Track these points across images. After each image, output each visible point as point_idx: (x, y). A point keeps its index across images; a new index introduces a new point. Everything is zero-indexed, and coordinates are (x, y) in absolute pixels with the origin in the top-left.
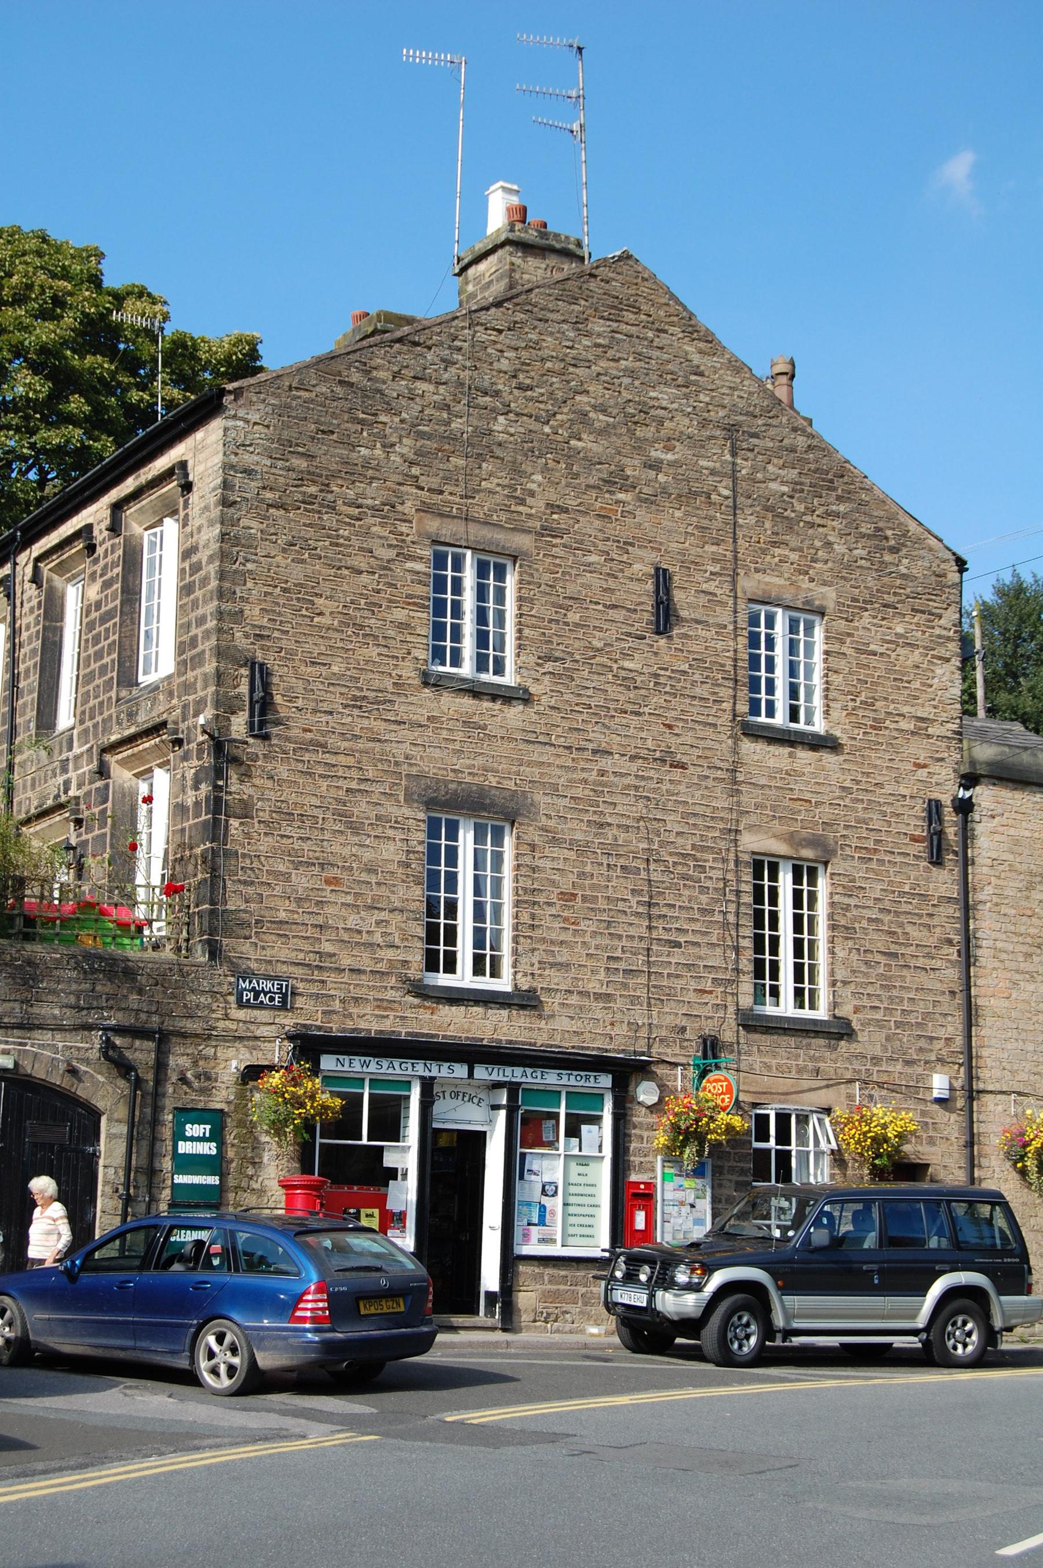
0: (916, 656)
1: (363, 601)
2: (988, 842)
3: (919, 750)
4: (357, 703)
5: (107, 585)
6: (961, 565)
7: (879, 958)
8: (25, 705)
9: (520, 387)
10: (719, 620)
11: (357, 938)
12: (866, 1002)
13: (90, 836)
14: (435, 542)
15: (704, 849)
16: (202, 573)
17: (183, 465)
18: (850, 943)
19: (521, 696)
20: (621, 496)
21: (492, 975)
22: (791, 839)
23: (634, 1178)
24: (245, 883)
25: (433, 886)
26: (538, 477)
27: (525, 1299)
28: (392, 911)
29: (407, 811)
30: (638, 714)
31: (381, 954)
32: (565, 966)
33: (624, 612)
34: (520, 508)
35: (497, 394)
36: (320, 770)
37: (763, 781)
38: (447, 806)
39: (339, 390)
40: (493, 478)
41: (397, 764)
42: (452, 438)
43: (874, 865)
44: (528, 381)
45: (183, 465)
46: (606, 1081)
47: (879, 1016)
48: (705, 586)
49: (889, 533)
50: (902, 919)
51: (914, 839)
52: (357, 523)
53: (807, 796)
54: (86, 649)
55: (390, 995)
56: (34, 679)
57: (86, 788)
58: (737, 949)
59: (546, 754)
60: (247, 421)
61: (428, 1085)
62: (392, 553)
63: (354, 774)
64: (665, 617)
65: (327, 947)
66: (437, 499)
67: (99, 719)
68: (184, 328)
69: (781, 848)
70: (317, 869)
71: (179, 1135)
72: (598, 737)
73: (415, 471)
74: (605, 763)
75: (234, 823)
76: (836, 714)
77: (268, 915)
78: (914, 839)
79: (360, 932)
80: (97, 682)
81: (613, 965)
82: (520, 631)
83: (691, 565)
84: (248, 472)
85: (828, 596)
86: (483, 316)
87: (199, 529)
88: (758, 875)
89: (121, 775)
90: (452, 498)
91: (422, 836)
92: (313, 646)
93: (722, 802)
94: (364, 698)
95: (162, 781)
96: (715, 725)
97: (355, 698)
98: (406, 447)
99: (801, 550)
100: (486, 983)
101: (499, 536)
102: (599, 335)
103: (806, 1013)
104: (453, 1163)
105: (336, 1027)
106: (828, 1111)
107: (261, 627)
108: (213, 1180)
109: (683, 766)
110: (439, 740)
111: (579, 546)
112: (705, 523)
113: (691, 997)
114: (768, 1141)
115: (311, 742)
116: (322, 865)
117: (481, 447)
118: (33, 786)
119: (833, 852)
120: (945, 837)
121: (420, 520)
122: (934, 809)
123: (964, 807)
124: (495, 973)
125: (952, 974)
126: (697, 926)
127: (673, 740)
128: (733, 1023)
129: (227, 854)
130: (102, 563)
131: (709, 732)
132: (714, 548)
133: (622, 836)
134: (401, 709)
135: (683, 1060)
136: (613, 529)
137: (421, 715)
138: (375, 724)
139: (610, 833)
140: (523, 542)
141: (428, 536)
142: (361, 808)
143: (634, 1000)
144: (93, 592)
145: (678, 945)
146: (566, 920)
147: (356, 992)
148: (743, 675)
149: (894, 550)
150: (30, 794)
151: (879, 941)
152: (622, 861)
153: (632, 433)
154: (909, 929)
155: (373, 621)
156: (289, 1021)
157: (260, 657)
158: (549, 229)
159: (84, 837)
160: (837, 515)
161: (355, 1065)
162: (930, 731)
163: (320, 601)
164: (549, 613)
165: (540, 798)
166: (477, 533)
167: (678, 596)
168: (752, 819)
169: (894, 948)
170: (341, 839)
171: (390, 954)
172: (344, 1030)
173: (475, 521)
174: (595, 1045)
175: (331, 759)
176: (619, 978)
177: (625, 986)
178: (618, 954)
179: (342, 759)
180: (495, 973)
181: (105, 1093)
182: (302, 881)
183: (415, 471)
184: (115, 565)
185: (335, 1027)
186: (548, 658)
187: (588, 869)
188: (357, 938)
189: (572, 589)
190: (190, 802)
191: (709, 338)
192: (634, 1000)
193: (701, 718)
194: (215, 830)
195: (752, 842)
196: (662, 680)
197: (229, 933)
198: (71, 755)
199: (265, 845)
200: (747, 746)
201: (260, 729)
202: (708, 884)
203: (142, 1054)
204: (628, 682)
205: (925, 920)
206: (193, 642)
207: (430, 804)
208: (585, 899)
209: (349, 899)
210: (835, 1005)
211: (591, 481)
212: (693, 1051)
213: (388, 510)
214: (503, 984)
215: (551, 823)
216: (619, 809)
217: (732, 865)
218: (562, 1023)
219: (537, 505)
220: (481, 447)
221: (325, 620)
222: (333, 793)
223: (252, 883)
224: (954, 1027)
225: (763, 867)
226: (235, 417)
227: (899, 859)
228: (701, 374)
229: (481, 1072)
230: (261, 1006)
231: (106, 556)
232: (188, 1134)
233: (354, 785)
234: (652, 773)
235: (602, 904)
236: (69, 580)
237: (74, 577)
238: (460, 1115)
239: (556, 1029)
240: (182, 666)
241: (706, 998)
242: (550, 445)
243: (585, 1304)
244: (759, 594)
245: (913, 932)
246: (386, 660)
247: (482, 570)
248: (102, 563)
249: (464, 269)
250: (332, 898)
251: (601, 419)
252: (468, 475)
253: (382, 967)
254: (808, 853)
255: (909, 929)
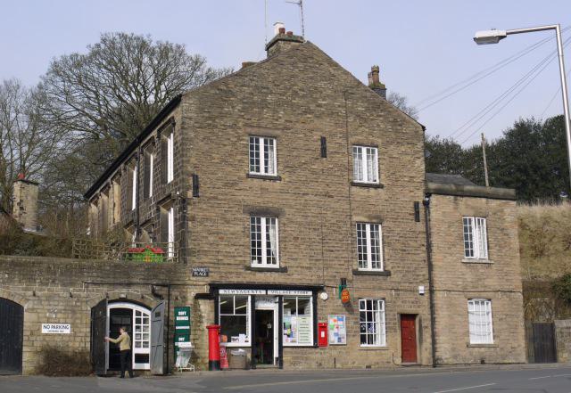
0: (409, 158)
4: (226, 185)
6: (424, 128)
17: (173, 117)
20: (310, 116)
22: (369, 217)
23: (320, 322)
25: (253, 238)
35: (268, 88)
38: (256, 213)
40: (267, 114)
45: (173, 117)
46: (310, 293)
47: (400, 269)
59: (288, 196)
61: (253, 297)
62: (235, 139)
63: (227, 206)
64: (324, 153)
65: (220, 258)
66: (250, 122)
69: (366, 220)
71: (176, 315)
72: (304, 190)
73: (243, 114)
74: (307, 197)
75: (190, 223)
76: (383, 176)
83: (333, 135)
84: (190, 119)
85: (379, 141)
86: (263, 65)
88: (359, 228)
89: (163, 210)
90: (254, 120)
92: (212, 169)
100: (271, 266)
103: (376, 270)
104: (262, 318)
105: (224, 281)
108: (188, 327)
119: (383, 220)
120: (420, 212)
122: (416, 205)
123: (426, 204)
124: (274, 263)
125: (424, 255)
133: (313, 219)
140: (278, 132)
141: (247, 133)
142: (229, 216)
143: (319, 268)
145: (332, 251)
151: (398, 246)
153: (312, 96)
156: (208, 280)
157: (196, 173)
160: (381, 116)
161: (230, 292)
163: (214, 155)
164: (287, 154)
166: (262, 131)
167: (328, 144)
171: (240, 259)
174: (305, 282)
175: (219, 202)
179: (223, 202)
180: (274, 263)
182: (211, 239)
183: (243, 114)
186: (288, 167)
189: (294, 146)
192: (319, 268)
199: (199, 228)
201: (196, 194)
204: (313, 173)
207: (251, 213)
210: (384, 267)
212: (339, 284)
215: (291, 216)
217: (349, 226)
218: (295, 276)
219: (282, 121)
220: (264, 105)
221: (217, 161)
224: (425, 272)
229: (270, 292)
239: (295, 278)
245: (411, 243)
251: (301, 93)
252: (260, 113)
253: (237, 262)
254: (374, 221)
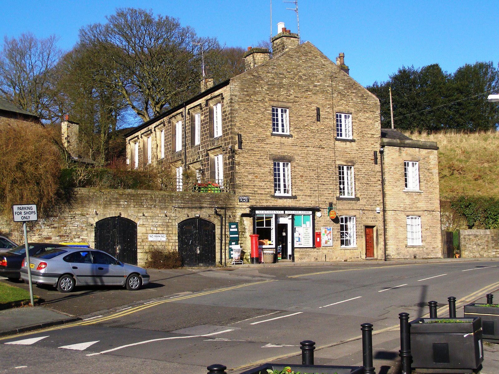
0: (371, 121)
1: (259, 120)
2: (387, 160)
3: (371, 141)
4: (258, 141)
5: (205, 117)
7: (365, 184)
8: (188, 139)
9: (288, 72)
10: (330, 117)
11: (261, 187)
12: (362, 193)
13: (205, 168)
14: (272, 107)
15: (329, 165)
16: (228, 116)
18: (359, 182)
19: (291, 136)
21: (288, 193)
22: (346, 161)
24: (240, 178)
26: (292, 91)
27: (296, 255)
28: (268, 181)
29: (269, 162)
30: (314, 138)
31: (266, 190)
33: (311, 117)
34: (289, 98)
35: (283, 74)
36: (252, 155)
37: (340, 150)
38: (277, 160)
39: (252, 77)
41: (267, 152)
43: (363, 166)
44: (290, 71)
45: (222, 94)
46: (311, 212)
48: (327, 111)
49: (365, 95)
50: (370, 176)
51: (372, 160)
52: (257, 104)
53: (349, 152)
54: (202, 129)
55: (269, 198)
56: (190, 134)
57: (204, 158)
59: (297, 148)
60: (234, 86)
62: (264, 110)
65: (256, 190)
66: (272, 97)
67: (206, 144)
69: (345, 164)
70: (253, 174)
71: (230, 228)
73: (268, 92)
74: (308, 149)
76: (355, 134)
77: (244, 184)
78: (372, 160)
79: (262, 186)
80: (205, 136)
81: (311, 189)
82: (290, 123)
85: (353, 110)
87: (226, 107)
88: (340, 169)
90: (275, 96)
91: (273, 166)
92: (250, 130)
94: (260, 139)
95: (221, 157)
96: (330, 139)
97: (258, 140)
99: (346, 101)
100: (286, 195)
101: (285, 104)
102: (303, 59)
105: (258, 205)
106: (355, 216)
107: (239, 127)
108: (237, 236)
109: (324, 148)
110: (275, 146)
111: (301, 104)
112: (327, 97)
113: (327, 195)
114: (343, 223)
115: (251, 149)
116: (254, 174)
117: (281, 86)
118: (191, 157)
119: (355, 164)
121: (269, 102)
122: (375, 153)
123: (382, 152)
125: (380, 187)
126: (328, 181)
127: (321, 143)
128: (336, 200)
129: (236, 173)
130: (204, 112)
131: (329, 141)
132: (329, 102)
134: (267, 141)
135: (326, 208)
136: (308, 100)
137: (271, 142)
138: (261, 143)
139: (309, 163)
140: (290, 105)
142: (260, 162)
144: (203, 117)
145: (324, 185)
146: (302, 181)
147: (262, 198)
148: (335, 128)
149: (366, 99)
150: (190, 158)
151: (364, 181)
152: (312, 168)
153: (311, 79)
154: (371, 178)
155: (261, 124)
156: (249, 204)
157: (240, 133)
158: (291, 32)
159: (204, 168)
160: (354, 93)
162: (374, 137)
165: (296, 157)
166: (280, 104)
167: (321, 113)
168: (338, 158)
169: (368, 182)
170: (257, 168)
171: (268, 190)
172: (260, 206)
173: (280, 101)
174: (308, 205)
175: (254, 152)
176: (312, 192)
177: (314, 193)
178: (312, 187)
179: (257, 152)
181: (216, 221)
182: (250, 177)
184: (207, 112)
185: (258, 205)
186: (296, 128)
187: (306, 170)
188: (261, 187)
189: (300, 113)
190: (228, 162)
191: (326, 58)
193: (327, 138)
194: (232, 168)
195: (338, 163)
196: (319, 131)
197: (237, 188)
198: (200, 151)
199: (243, 170)
200: (337, 142)
201: (240, 147)
202: (330, 172)
203: (222, 212)
205: (374, 176)
206: (226, 130)
207: (274, 160)
208: (305, 176)
209: (259, 180)
210: (355, 195)
211: (303, 91)
213: (263, 101)
214: (290, 195)
215: (298, 162)
216: (312, 158)
218: (302, 202)
219: (292, 97)
220: (281, 86)
222: (255, 159)
223: (241, 178)
224: (380, 198)
225: (340, 168)
226: (232, 85)
227: (368, 164)
228: (325, 65)
231: (205, 110)
232: (232, 227)
233: (259, 157)
234: (317, 150)
235: (309, 177)
236: (196, 114)
237: (197, 113)
238: (282, 221)
241: (330, 195)
242: (294, 84)
243: (308, 256)
244: (338, 111)
246: (264, 131)
247: (282, 111)
248: (204, 112)
249: (273, 41)
250: (256, 180)
251: (304, 77)
253: (266, 193)
255: (371, 178)
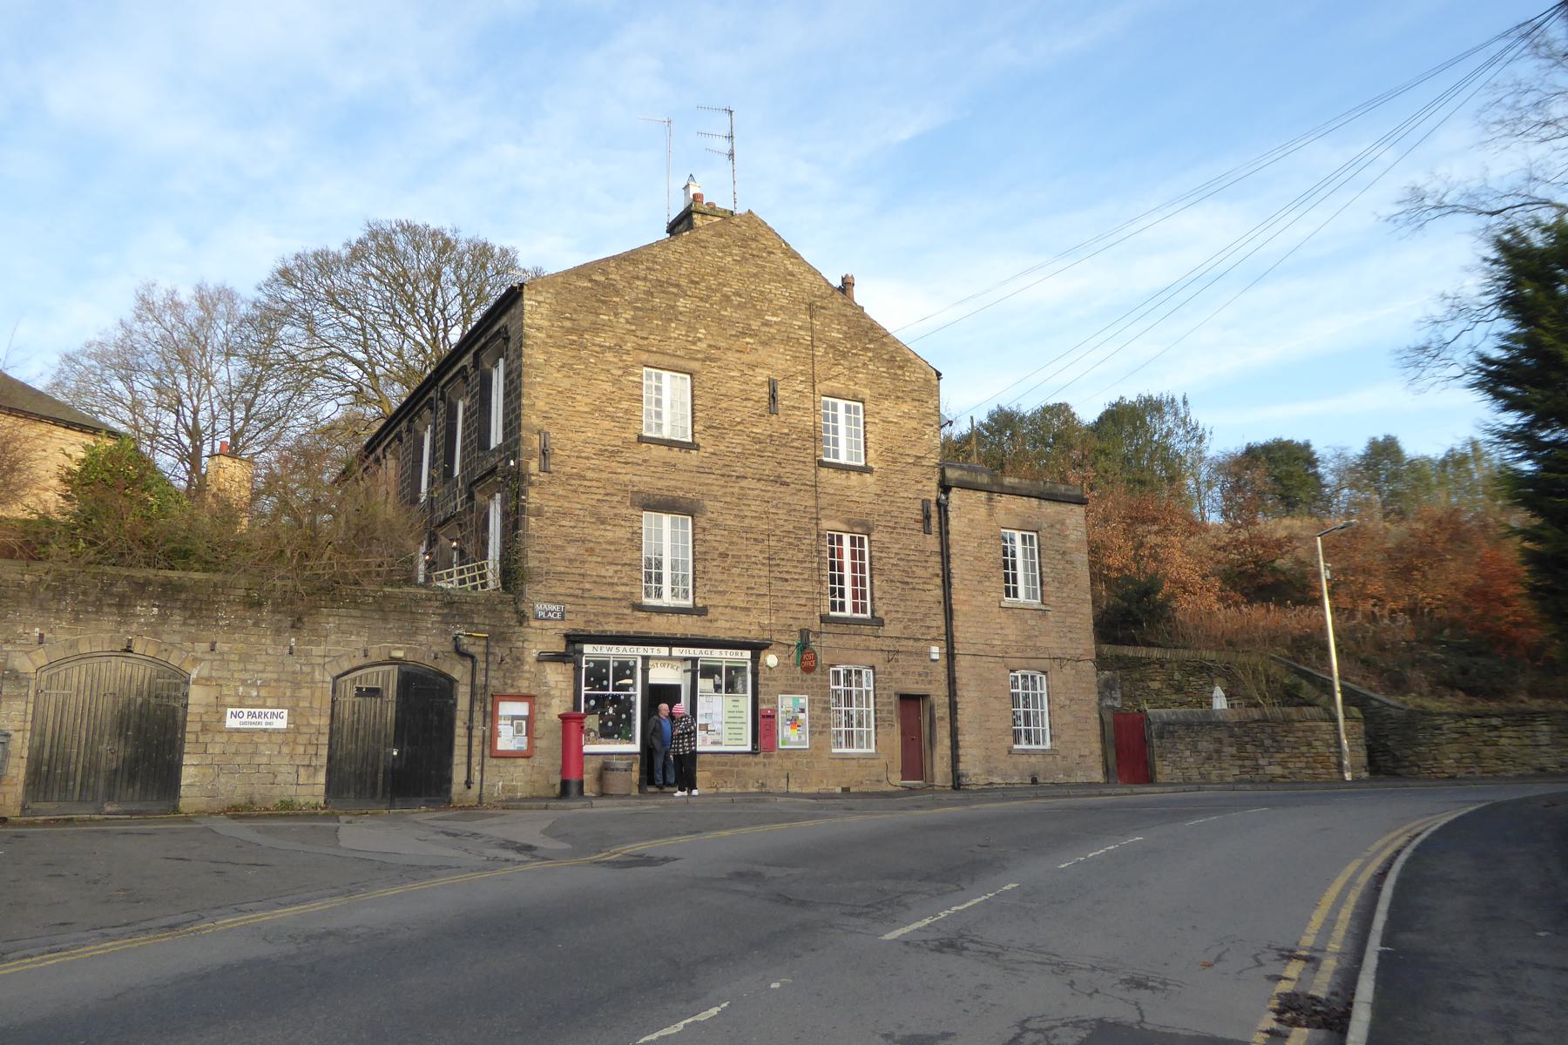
6: (939, 374)
22: (848, 522)
32: (724, 593)
40: (676, 330)
42: (653, 309)
46: (747, 654)
58: (820, 582)
59: (710, 479)
65: (587, 586)
68: (469, 236)
74: (744, 483)
85: (866, 393)
89: (479, 498)
93: (812, 503)
98: (629, 315)
113: (793, 608)
117: (671, 315)
122: (925, 503)
125: (939, 592)
139: (747, 522)
142: (605, 510)
149: (901, 367)
157: (546, 429)
160: (869, 350)
165: (708, 503)
168: (827, 512)
171: (623, 589)
174: (739, 635)
176: (753, 598)
182: (571, 550)
189: (723, 391)
191: (795, 256)
218: (722, 624)
220: (671, 315)
224: (940, 621)
230: (549, 619)
240: (505, 438)
